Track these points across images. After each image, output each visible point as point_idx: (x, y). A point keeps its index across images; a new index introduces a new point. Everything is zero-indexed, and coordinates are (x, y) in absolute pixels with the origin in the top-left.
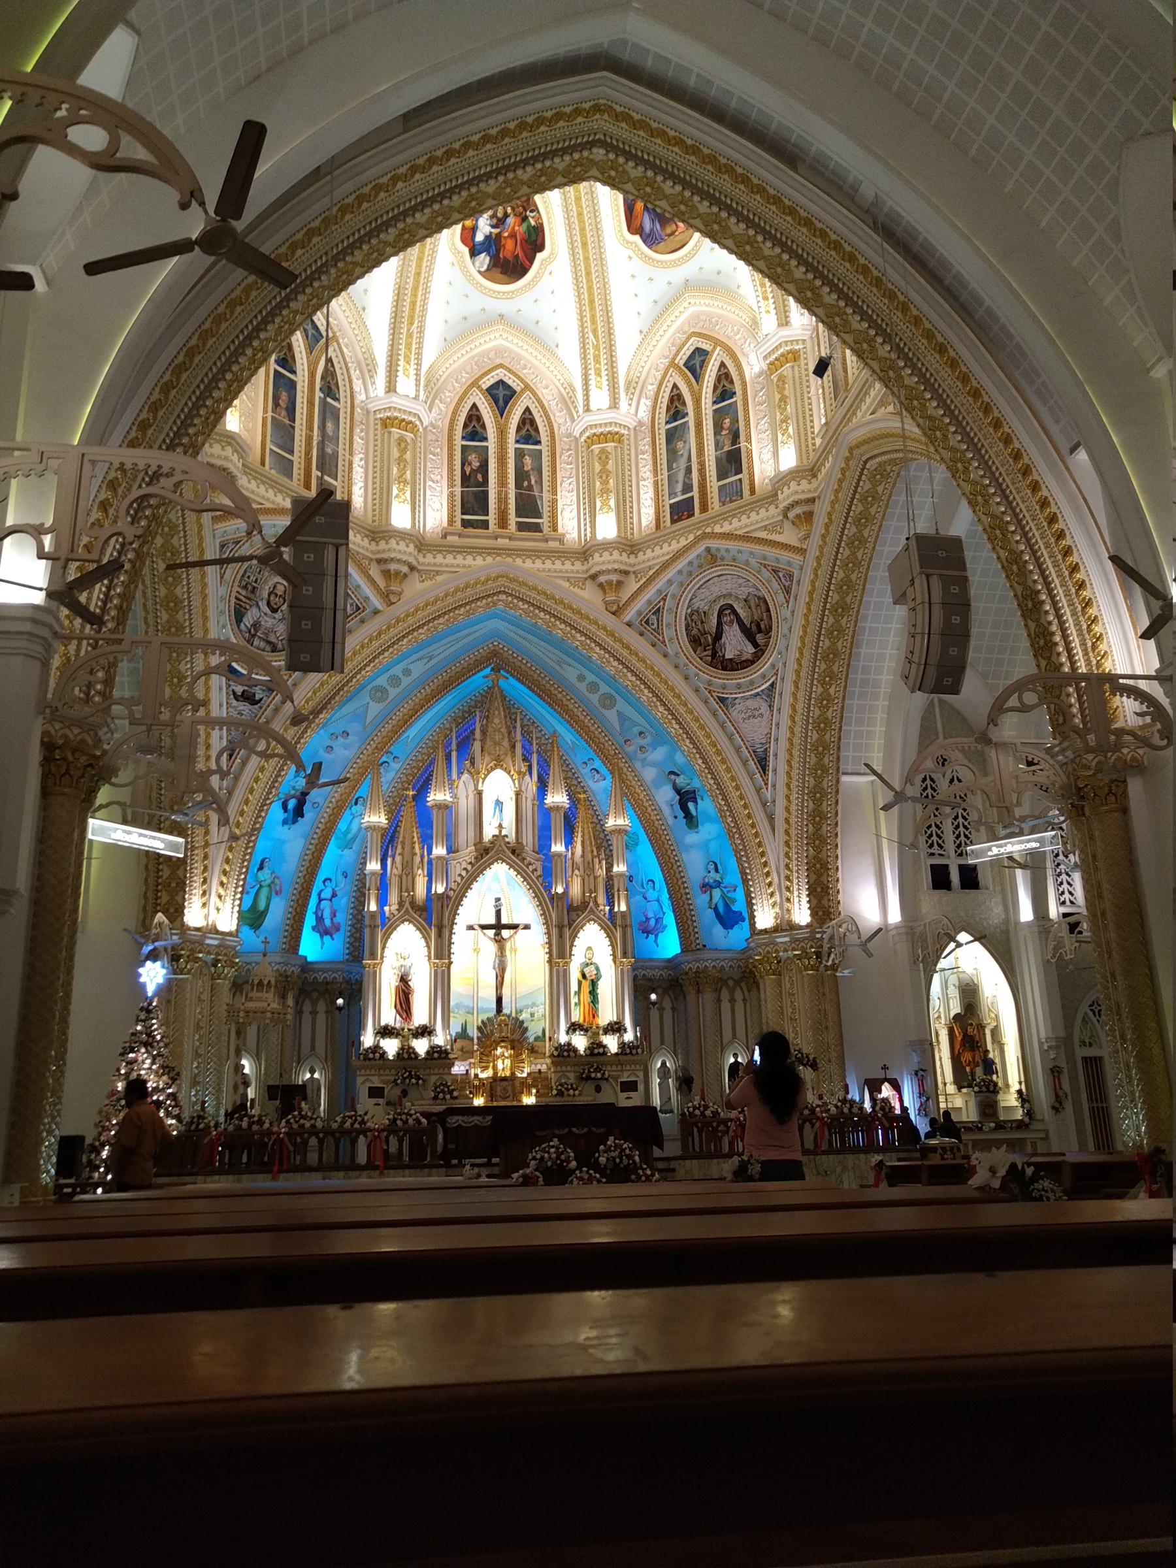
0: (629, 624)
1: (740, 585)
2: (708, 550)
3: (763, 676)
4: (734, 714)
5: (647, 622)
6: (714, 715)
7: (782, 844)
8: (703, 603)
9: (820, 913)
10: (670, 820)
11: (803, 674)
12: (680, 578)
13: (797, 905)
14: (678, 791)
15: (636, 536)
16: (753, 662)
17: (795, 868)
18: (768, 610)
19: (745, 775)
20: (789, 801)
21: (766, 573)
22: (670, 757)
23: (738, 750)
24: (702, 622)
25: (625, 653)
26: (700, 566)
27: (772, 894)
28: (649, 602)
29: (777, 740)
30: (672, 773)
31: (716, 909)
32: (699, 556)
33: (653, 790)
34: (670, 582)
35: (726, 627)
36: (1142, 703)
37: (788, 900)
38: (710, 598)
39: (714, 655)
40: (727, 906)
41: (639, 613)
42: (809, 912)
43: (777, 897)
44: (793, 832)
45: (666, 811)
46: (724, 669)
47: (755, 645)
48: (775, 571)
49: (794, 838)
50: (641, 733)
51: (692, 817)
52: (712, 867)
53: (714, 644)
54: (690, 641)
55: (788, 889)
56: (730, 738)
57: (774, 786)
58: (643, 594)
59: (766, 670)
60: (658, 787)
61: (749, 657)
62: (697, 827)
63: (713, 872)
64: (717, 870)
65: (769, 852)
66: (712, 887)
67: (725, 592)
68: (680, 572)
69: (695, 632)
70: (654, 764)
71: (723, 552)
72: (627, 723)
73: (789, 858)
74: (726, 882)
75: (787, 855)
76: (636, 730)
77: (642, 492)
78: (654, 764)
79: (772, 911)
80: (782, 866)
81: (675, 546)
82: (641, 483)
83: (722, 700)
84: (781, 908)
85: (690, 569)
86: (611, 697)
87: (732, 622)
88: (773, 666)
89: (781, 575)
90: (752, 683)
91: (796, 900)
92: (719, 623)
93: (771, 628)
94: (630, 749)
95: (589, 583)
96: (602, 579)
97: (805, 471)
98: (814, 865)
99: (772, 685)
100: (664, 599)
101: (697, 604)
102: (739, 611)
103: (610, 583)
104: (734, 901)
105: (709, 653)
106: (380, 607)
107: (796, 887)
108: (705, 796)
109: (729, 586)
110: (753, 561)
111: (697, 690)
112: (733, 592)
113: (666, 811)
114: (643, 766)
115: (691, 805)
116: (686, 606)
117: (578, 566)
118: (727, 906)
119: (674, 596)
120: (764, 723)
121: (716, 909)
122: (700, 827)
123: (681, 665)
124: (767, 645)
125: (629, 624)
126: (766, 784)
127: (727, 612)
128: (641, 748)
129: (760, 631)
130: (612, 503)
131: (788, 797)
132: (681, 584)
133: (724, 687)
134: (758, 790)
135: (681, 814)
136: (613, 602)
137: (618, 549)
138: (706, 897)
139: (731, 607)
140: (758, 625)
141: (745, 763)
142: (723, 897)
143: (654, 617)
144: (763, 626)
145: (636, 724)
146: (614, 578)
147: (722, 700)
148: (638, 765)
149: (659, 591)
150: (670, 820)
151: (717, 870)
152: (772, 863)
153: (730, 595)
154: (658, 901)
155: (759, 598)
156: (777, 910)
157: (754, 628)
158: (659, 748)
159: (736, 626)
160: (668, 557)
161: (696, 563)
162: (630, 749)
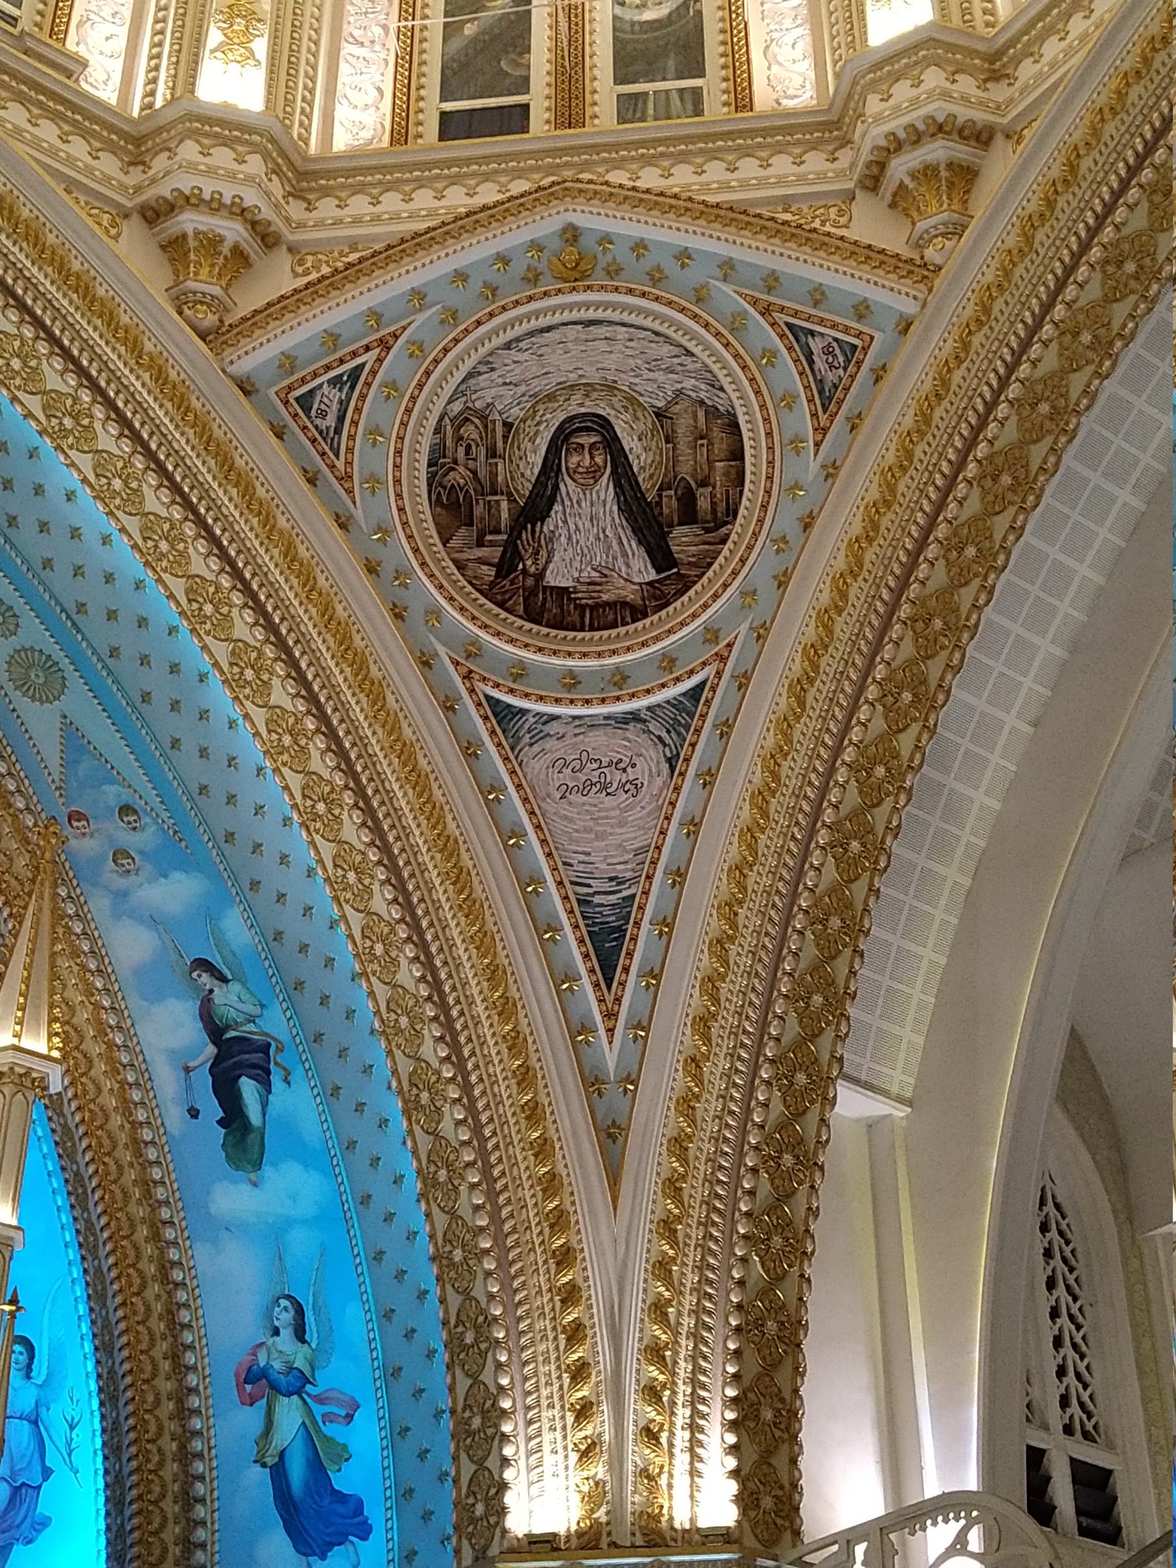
0: (246, 387)
1: (654, 364)
2: (572, 234)
3: (668, 662)
4: (536, 767)
5: (305, 402)
6: (470, 751)
7: (645, 1227)
8: (508, 393)
9: (767, 1502)
10: (174, 1118)
11: (829, 664)
12: (457, 297)
13: (682, 1460)
14: (215, 1029)
15: (313, 149)
16: (638, 613)
17: (688, 1322)
18: (737, 454)
19: (538, 969)
20: (698, 1079)
21: (764, 333)
22: (209, 915)
23: (529, 882)
24: (492, 453)
25: (205, 470)
26: (532, 278)
27: (584, 1412)
28: (332, 338)
29: (679, 876)
30: (203, 965)
31: (279, 1473)
32: (536, 246)
33: (134, 1003)
34: (419, 296)
35: (568, 487)
36: (505, 1462)
37: (650, 1435)
38: (536, 386)
39: (507, 565)
40: (317, 1469)
41: (288, 362)
42: (733, 1487)
43: (601, 1424)
44: (695, 1191)
45: (167, 1081)
46: (533, 616)
47: (661, 557)
48: (797, 334)
49: (698, 1212)
50: (126, 810)
51: (246, 1126)
52: (284, 1318)
53: (516, 529)
54: (436, 502)
55: (652, 1393)
56: (511, 835)
57: (641, 1025)
58: (320, 304)
59: (686, 644)
60: (156, 996)
61: (630, 594)
62: (258, 1165)
63: (286, 1334)
64: (300, 1334)
65: (588, 1251)
66: (275, 1388)
67: (595, 378)
68: (461, 276)
69: (459, 477)
70: (154, 921)
71: (621, 253)
72: (85, 767)
73: (667, 1279)
74: (325, 1380)
75: (662, 1269)
76: (113, 794)
77: (344, 68)
78: (154, 921)
79: (576, 1477)
80: (636, 1306)
81: (457, 199)
82: (347, 49)
83: (502, 715)
84: (616, 1464)
85: (492, 276)
86: (50, 666)
87: (594, 473)
88: (711, 634)
89: (816, 345)
90: (620, 678)
91: (682, 1437)
92: (551, 468)
93: (732, 512)
94: (85, 846)
95: (132, 229)
96: (189, 221)
97: (972, 53)
98: (759, 1324)
99: (695, 694)
100: (385, 345)
101: (488, 392)
102: (629, 442)
103: (212, 243)
104: (342, 1454)
105: (495, 553)
106: (909, 307)
107: (683, 1390)
108: (298, 1074)
109: (611, 361)
110: (727, 293)
111: (426, 662)
112: (624, 382)
113: (167, 1081)
114: (117, 916)
115: (248, 1088)
116: (449, 389)
117: (109, 164)
118: (317, 1469)
119: (418, 348)
120: (642, 810)
121: (279, 1473)
122: (267, 1170)
123: (387, 571)
124: (704, 564)
125: (246, 387)
126: (610, 1016)
127: (587, 440)
128: (120, 854)
129: (689, 514)
130: (261, 46)
131: (694, 1064)
132: (452, 316)
133: (519, 672)
134: (580, 1030)
135: (213, 1110)
136: (212, 302)
137: (266, 156)
138: (250, 1419)
139: (604, 425)
140: (688, 500)
141: (545, 928)
142: (310, 1432)
143: (335, 395)
144: (703, 503)
145: (112, 775)
146: (233, 231)
147: (502, 715)
148: (99, 905)
149: (375, 315)
150: (174, 1118)
151: (300, 1334)
152: (596, 1293)
153: (611, 388)
154: (35, 1422)
155: (712, 412)
156: (599, 1470)
157: (670, 505)
158: (177, 875)
159: (605, 489)
160: (422, 226)
161: (519, 266)
162: (85, 846)
